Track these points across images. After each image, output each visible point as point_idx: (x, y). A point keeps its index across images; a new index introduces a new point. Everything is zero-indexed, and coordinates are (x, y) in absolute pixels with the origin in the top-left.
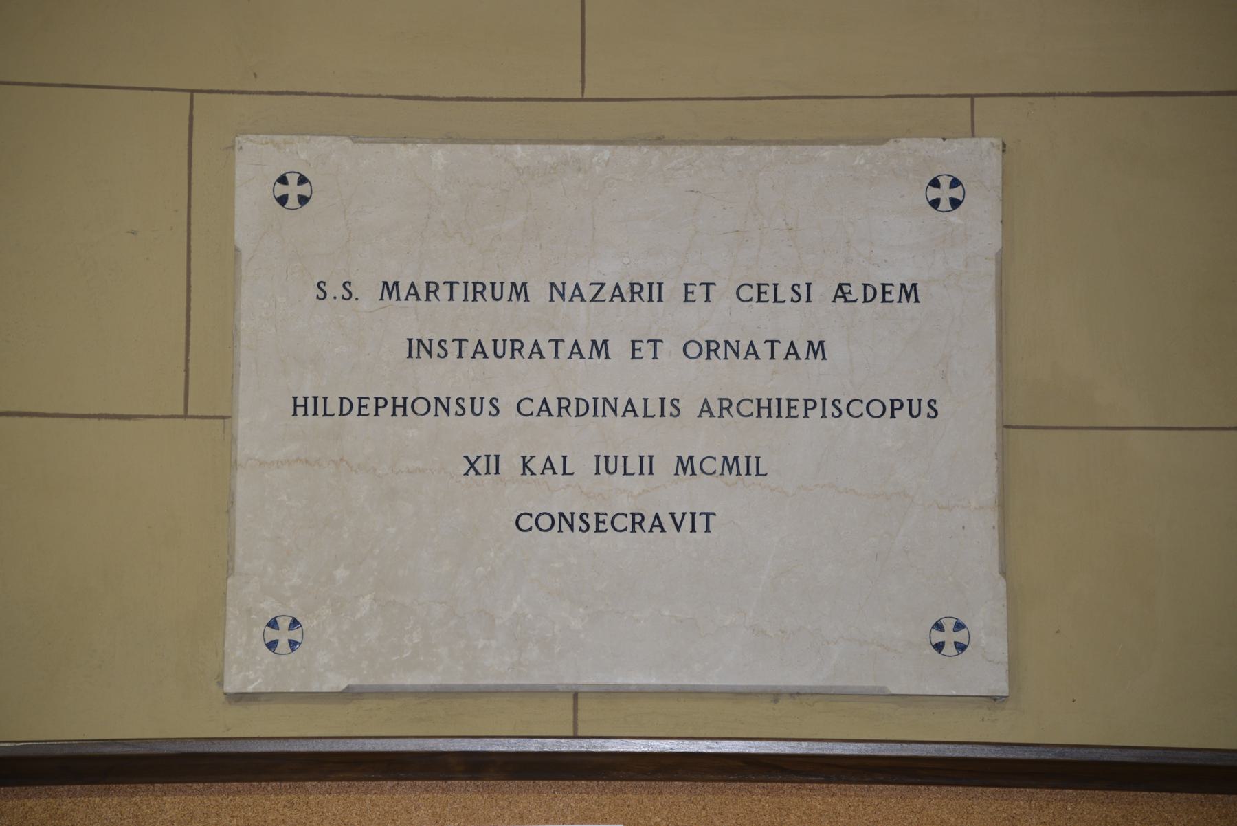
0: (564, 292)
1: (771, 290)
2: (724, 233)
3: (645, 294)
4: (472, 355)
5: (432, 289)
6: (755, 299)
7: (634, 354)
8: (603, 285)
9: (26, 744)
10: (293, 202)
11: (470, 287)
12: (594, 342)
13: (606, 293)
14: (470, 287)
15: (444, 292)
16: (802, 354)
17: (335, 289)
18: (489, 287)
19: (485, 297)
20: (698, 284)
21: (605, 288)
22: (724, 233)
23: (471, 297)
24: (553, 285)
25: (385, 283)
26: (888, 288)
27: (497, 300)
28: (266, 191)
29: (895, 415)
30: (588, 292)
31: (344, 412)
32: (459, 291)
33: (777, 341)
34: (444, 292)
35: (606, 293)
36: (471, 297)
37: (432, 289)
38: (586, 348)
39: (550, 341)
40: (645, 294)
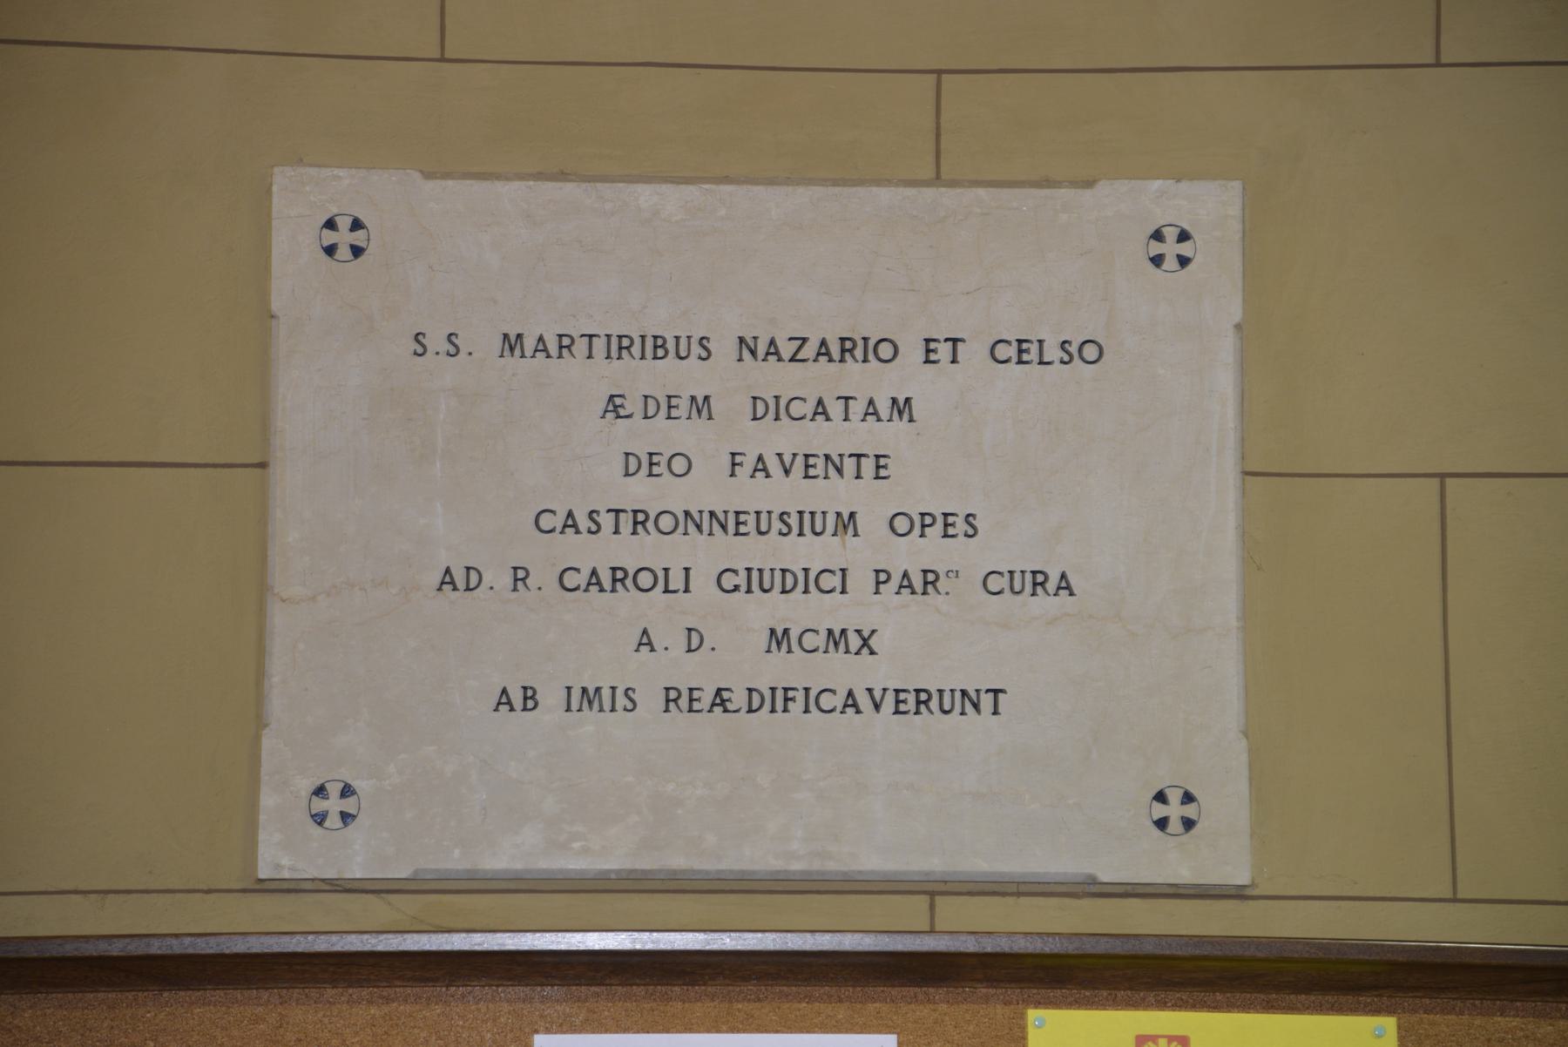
0: (756, 346)
1: (1034, 348)
2: (979, 289)
3: (636, 350)
4: (601, 414)
5: (565, 345)
6: (1015, 359)
7: (669, 413)
8: (804, 340)
9: (1435, 944)
10: (1171, 234)
11: (614, 341)
12: (894, 401)
13: (809, 351)
14: (614, 341)
15: (581, 346)
16: (884, 414)
17: (436, 342)
18: (638, 341)
19: (574, 352)
20: (942, 340)
21: (808, 344)
22: (979, 289)
23: (614, 353)
24: (741, 340)
25: (506, 336)
26: (1025, 346)
27: (682, 358)
28: (310, 238)
29: (737, 473)
30: (787, 350)
31: (631, 471)
32: (599, 344)
33: (851, 398)
34: (581, 346)
35: (809, 351)
36: (614, 353)
37: (565, 345)
38: (884, 407)
39: (839, 398)
40: (636, 350)
